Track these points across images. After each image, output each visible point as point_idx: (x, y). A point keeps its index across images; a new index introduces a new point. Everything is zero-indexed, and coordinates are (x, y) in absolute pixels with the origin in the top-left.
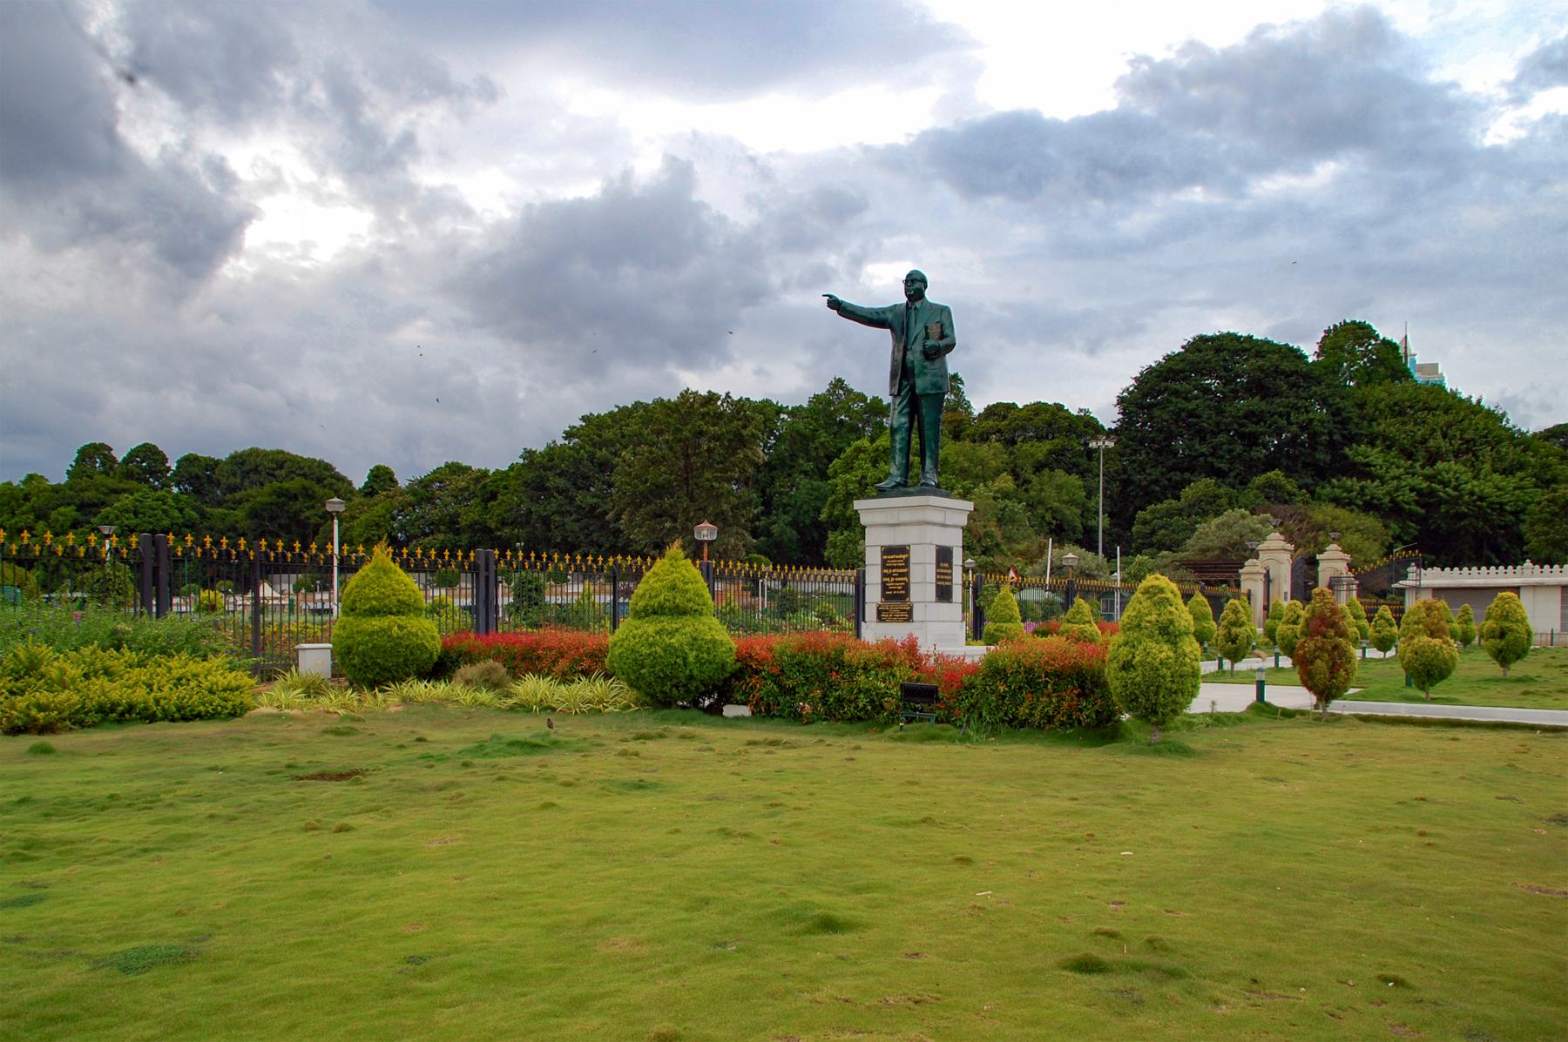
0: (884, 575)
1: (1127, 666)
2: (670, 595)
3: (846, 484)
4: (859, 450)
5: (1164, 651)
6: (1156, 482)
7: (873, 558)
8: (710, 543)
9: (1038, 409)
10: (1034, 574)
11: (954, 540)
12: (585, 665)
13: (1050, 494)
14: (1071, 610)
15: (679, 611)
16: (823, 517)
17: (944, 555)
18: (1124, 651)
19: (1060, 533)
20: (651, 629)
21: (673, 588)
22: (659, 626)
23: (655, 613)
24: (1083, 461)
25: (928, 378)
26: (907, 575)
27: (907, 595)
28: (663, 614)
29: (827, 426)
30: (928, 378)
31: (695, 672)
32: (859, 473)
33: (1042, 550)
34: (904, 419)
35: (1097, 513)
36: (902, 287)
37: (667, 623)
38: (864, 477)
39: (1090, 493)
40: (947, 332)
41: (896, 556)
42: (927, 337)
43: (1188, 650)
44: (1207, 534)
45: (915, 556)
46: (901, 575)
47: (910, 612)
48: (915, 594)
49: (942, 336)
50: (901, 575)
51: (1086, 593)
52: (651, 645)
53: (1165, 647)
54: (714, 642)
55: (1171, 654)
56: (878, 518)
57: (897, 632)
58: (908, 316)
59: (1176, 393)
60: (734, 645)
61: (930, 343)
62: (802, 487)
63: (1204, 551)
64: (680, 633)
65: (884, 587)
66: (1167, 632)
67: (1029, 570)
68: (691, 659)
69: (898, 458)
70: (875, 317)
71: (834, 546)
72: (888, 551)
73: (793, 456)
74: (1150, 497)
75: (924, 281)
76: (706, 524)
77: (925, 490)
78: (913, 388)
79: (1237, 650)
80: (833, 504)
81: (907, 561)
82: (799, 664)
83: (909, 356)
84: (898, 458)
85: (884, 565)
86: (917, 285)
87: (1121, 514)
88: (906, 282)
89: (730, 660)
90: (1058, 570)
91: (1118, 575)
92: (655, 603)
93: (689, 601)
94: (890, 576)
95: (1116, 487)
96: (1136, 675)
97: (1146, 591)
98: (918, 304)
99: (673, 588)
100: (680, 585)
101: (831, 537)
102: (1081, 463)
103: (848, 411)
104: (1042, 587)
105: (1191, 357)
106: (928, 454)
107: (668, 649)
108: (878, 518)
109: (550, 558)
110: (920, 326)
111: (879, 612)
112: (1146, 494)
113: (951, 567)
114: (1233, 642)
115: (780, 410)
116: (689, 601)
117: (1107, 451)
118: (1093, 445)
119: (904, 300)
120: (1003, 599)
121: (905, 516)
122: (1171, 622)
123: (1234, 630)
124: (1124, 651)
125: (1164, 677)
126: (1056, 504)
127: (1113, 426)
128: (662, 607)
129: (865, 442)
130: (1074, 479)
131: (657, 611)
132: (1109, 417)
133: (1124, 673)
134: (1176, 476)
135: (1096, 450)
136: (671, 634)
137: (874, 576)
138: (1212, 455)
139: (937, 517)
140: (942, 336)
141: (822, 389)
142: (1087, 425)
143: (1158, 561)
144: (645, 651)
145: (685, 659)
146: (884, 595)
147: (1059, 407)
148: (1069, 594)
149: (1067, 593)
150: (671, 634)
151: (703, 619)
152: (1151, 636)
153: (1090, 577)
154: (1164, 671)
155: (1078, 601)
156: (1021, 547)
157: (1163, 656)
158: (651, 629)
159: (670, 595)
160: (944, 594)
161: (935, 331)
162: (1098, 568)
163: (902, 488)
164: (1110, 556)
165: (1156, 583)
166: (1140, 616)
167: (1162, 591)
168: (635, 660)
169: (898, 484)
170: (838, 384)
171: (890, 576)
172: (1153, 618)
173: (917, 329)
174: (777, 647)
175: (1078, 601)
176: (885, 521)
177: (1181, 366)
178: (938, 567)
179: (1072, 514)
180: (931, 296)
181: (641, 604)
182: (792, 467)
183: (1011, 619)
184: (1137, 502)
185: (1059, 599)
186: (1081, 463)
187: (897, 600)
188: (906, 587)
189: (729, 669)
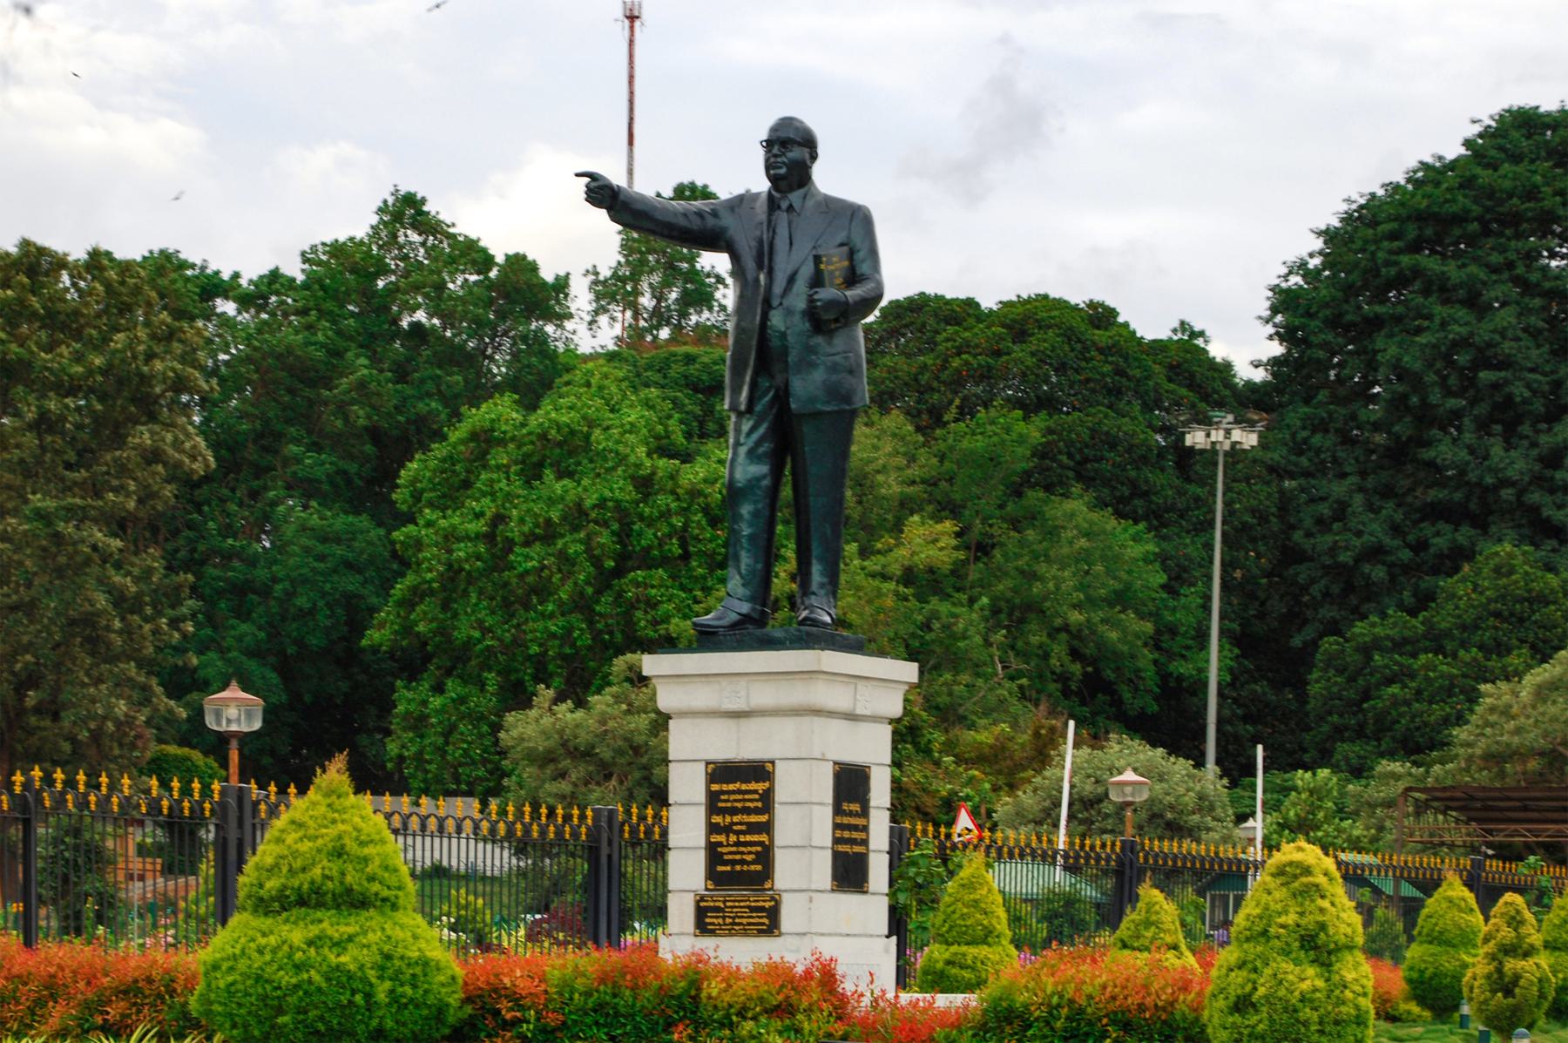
0: (712, 828)
1: (1242, 1005)
2: (334, 868)
3: (450, 537)
4: (485, 440)
5: (1309, 979)
6: (1376, 553)
7: (687, 788)
8: (244, 738)
9: (1032, 319)
10: (1020, 818)
11: (873, 748)
12: (113, 1012)
13: (1058, 580)
14: (1131, 918)
15: (354, 901)
16: (375, 637)
17: (850, 784)
18: (1238, 977)
19: (1102, 696)
20: (297, 936)
21: (339, 853)
22: (314, 930)
23: (302, 902)
24: (1163, 480)
25: (818, 375)
26: (767, 828)
27: (767, 873)
28: (320, 905)
29: (370, 342)
30: (818, 375)
31: (389, 1023)
32: (488, 506)
33: (1043, 752)
34: (761, 469)
35: (1202, 637)
36: (759, 155)
37: (331, 925)
38: (499, 519)
39: (1179, 576)
40: (864, 268)
41: (742, 789)
42: (817, 281)
43: (1349, 976)
44: (1506, 712)
45: (786, 787)
46: (753, 828)
47: (774, 914)
48: (786, 872)
49: (853, 278)
50: (753, 828)
51: (1169, 876)
52: (298, 967)
53: (1311, 971)
54: (425, 963)
55: (1320, 983)
56: (702, 697)
57: (741, 953)
58: (771, 226)
59: (1442, 289)
60: (459, 972)
61: (826, 294)
62: (297, 528)
63: (1495, 758)
64: (360, 943)
65: (713, 855)
66: (1316, 946)
67: (1004, 806)
68: (381, 997)
69: (745, 559)
70: (696, 224)
71: (418, 723)
72: (721, 772)
73: (269, 439)
74: (1355, 594)
75: (808, 143)
76: (234, 692)
77: (810, 636)
78: (782, 396)
79: (1515, 1010)
80: (409, 603)
81: (767, 799)
82: (599, 1007)
83: (776, 320)
84: (745, 559)
85: (713, 803)
86: (796, 153)
87: (1267, 650)
88: (769, 144)
89: (454, 1000)
90: (1088, 807)
91: (1257, 825)
92: (302, 881)
93: (371, 879)
94: (727, 830)
95: (1257, 559)
96: (1258, 1021)
97: (1280, 872)
98: (795, 197)
99: (339, 853)
100: (351, 846)
101: (406, 699)
102: (1151, 488)
103: (437, 297)
104: (1048, 858)
105: (1485, 176)
106: (816, 549)
107: (336, 974)
108: (702, 697)
109: (70, 783)
110: (803, 251)
111: (701, 913)
112: (1349, 588)
113: (865, 812)
114: (1508, 992)
115: (213, 287)
116: (371, 879)
117: (1235, 453)
118: (1196, 438)
119: (762, 185)
120: (970, 886)
121: (764, 695)
122: (1323, 927)
123: (1511, 965)
124: (1238, 977)
125: (1306, 1024)
126: (1076, 617)
127: (1259, 376)
128: (317, 890)
129: (501, 410)
130: (1133, 545)
131: (306, 900)
132: (1246, 347)
133: (1237, 1018)
134: (1441, 538)
135: (1211, 454)
136: (340, 945)
137: (687, 828)
138: (1538, 480)
139: (836, 697)
140: (853, 278)
141: (355, 222)
142: (1187, 370)
143: (1376, 791)
144: (287, 978)
145: (368, 996)
146: (712, 874)
147: (1102, 316)
148: (1124, 879)
149: (1119, 873)
150: (340, 945)
151: (399, 916)
152: (1286, 952)
153: (1176, 829)
154: (1307, 1013)
155: (1149, 893)
156: (984, 736)
157: (1305, 986)
158: (297, 936)
159: (334, 868)
160: (849, 873)
161: (836, 265)
162: (1205, 804)
163: (750, 632)
164: (1237, 770)
165: (1298, 856)
166: (1267, 916)
167: (1307, 871)
168: (264, 998)
169: (745, 619)
170: (406, 211)
171: (727, 830)
172: (1291, 919)
173: (791, 260)
174: (555, 975)
175: (1149, 893)
176: (711, 704)
177: (1463, 201)
178: (838, 810)
179: (1126, 632)
180: (828, 178)
181: (272, 884)
182: (260, 471)
183: (986, 937)
184: (1328, 612)
185: (1089, 892)
186: (1151, 488)
187: (742, 882)
188: (766, 856)
189: (451, 1020)
